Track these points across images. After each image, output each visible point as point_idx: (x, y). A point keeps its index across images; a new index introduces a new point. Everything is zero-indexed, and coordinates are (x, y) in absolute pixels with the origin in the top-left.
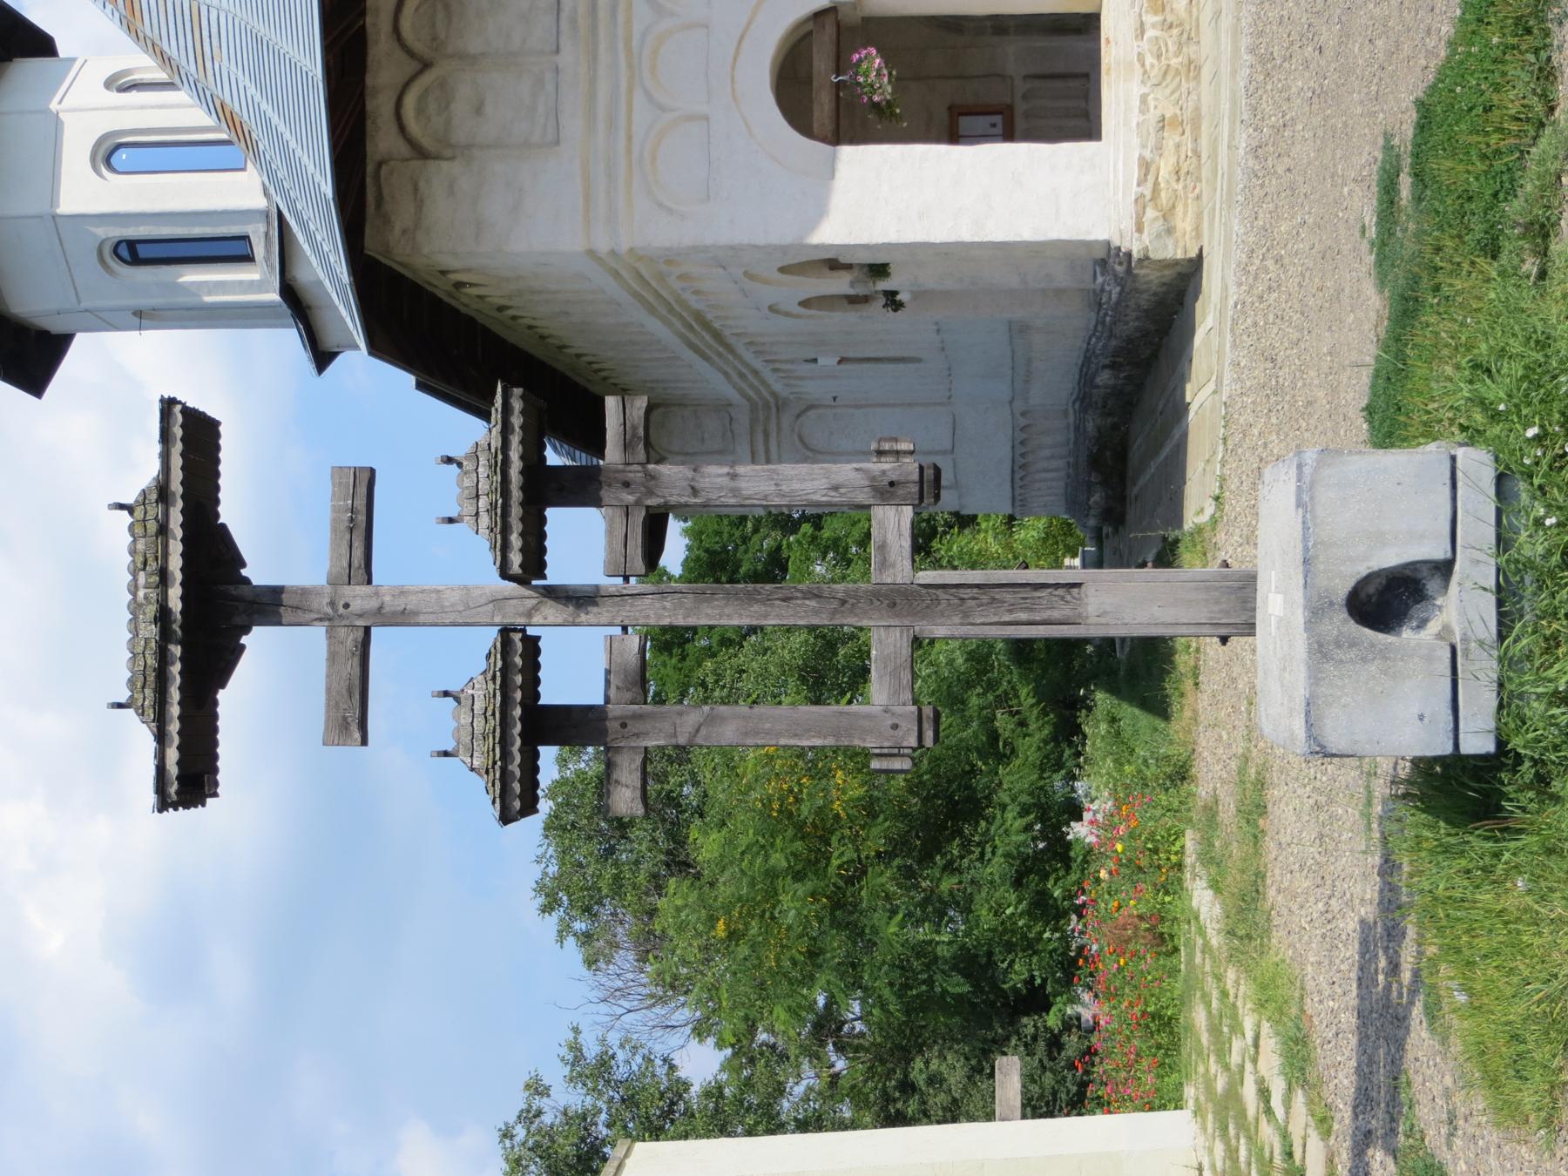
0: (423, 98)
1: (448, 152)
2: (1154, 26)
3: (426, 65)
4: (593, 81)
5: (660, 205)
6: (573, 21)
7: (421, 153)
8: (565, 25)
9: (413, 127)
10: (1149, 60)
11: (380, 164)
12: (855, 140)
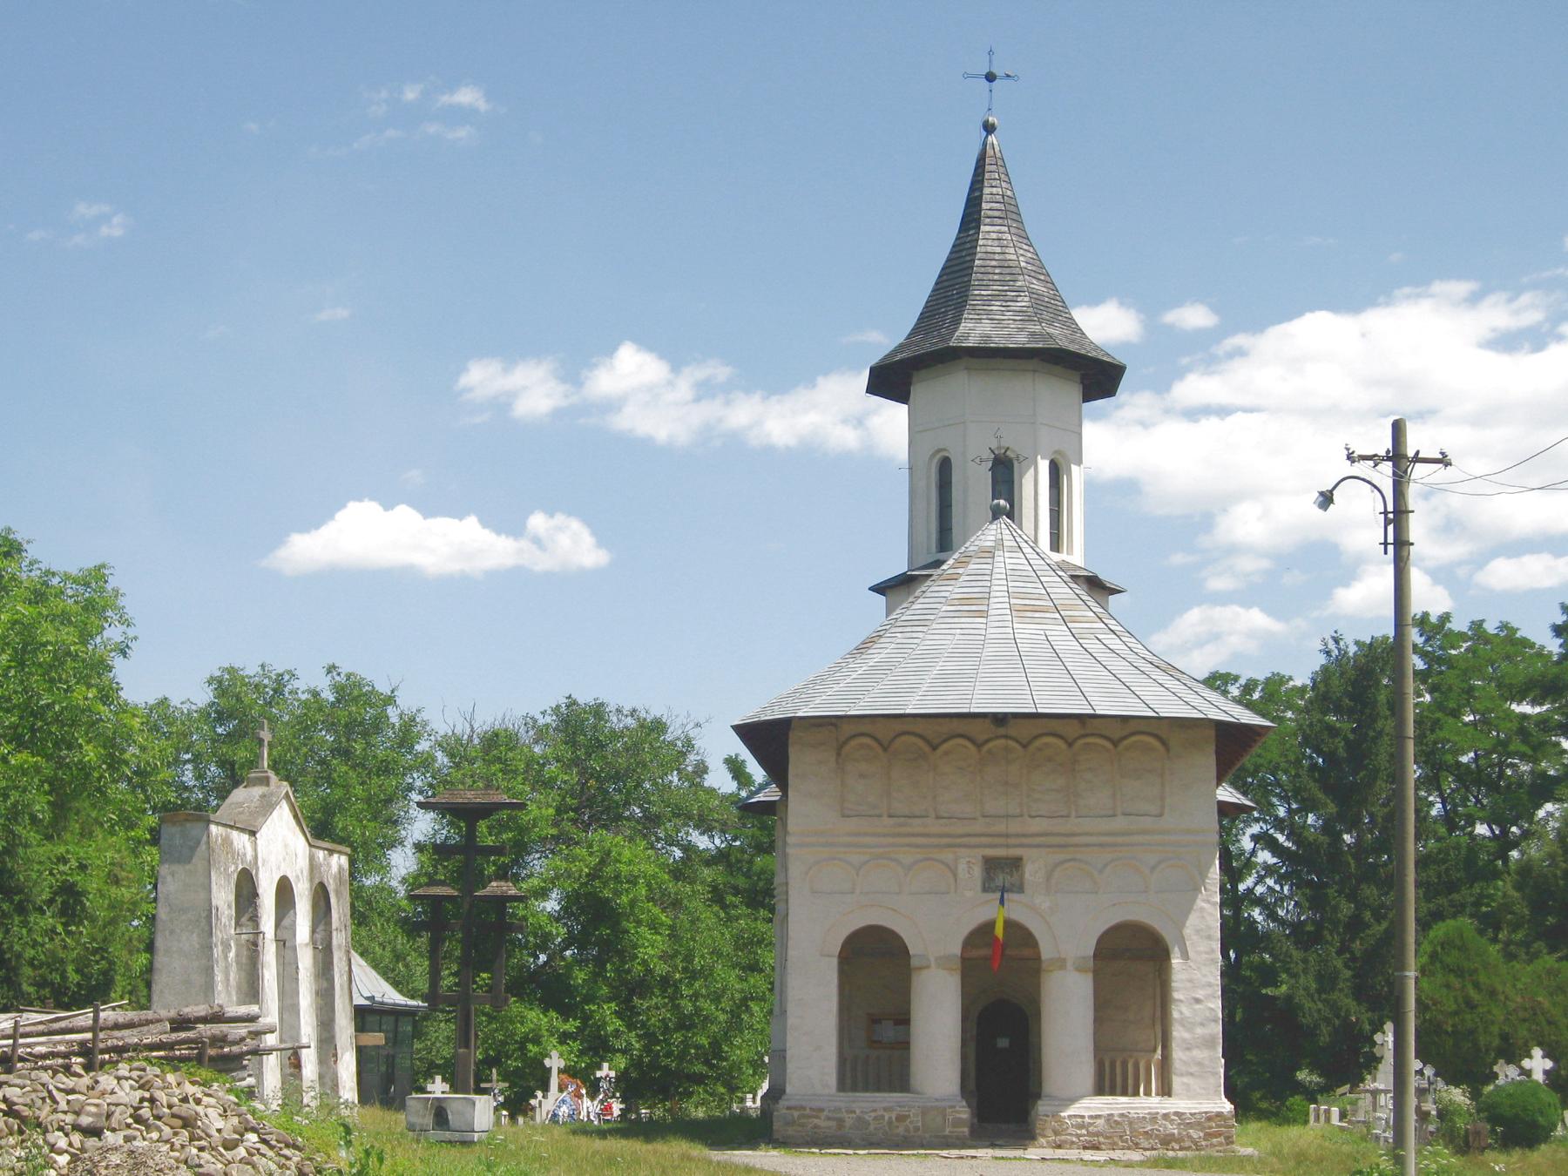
3: (885, 749)
6: (901, 825)
9: (853, 743)
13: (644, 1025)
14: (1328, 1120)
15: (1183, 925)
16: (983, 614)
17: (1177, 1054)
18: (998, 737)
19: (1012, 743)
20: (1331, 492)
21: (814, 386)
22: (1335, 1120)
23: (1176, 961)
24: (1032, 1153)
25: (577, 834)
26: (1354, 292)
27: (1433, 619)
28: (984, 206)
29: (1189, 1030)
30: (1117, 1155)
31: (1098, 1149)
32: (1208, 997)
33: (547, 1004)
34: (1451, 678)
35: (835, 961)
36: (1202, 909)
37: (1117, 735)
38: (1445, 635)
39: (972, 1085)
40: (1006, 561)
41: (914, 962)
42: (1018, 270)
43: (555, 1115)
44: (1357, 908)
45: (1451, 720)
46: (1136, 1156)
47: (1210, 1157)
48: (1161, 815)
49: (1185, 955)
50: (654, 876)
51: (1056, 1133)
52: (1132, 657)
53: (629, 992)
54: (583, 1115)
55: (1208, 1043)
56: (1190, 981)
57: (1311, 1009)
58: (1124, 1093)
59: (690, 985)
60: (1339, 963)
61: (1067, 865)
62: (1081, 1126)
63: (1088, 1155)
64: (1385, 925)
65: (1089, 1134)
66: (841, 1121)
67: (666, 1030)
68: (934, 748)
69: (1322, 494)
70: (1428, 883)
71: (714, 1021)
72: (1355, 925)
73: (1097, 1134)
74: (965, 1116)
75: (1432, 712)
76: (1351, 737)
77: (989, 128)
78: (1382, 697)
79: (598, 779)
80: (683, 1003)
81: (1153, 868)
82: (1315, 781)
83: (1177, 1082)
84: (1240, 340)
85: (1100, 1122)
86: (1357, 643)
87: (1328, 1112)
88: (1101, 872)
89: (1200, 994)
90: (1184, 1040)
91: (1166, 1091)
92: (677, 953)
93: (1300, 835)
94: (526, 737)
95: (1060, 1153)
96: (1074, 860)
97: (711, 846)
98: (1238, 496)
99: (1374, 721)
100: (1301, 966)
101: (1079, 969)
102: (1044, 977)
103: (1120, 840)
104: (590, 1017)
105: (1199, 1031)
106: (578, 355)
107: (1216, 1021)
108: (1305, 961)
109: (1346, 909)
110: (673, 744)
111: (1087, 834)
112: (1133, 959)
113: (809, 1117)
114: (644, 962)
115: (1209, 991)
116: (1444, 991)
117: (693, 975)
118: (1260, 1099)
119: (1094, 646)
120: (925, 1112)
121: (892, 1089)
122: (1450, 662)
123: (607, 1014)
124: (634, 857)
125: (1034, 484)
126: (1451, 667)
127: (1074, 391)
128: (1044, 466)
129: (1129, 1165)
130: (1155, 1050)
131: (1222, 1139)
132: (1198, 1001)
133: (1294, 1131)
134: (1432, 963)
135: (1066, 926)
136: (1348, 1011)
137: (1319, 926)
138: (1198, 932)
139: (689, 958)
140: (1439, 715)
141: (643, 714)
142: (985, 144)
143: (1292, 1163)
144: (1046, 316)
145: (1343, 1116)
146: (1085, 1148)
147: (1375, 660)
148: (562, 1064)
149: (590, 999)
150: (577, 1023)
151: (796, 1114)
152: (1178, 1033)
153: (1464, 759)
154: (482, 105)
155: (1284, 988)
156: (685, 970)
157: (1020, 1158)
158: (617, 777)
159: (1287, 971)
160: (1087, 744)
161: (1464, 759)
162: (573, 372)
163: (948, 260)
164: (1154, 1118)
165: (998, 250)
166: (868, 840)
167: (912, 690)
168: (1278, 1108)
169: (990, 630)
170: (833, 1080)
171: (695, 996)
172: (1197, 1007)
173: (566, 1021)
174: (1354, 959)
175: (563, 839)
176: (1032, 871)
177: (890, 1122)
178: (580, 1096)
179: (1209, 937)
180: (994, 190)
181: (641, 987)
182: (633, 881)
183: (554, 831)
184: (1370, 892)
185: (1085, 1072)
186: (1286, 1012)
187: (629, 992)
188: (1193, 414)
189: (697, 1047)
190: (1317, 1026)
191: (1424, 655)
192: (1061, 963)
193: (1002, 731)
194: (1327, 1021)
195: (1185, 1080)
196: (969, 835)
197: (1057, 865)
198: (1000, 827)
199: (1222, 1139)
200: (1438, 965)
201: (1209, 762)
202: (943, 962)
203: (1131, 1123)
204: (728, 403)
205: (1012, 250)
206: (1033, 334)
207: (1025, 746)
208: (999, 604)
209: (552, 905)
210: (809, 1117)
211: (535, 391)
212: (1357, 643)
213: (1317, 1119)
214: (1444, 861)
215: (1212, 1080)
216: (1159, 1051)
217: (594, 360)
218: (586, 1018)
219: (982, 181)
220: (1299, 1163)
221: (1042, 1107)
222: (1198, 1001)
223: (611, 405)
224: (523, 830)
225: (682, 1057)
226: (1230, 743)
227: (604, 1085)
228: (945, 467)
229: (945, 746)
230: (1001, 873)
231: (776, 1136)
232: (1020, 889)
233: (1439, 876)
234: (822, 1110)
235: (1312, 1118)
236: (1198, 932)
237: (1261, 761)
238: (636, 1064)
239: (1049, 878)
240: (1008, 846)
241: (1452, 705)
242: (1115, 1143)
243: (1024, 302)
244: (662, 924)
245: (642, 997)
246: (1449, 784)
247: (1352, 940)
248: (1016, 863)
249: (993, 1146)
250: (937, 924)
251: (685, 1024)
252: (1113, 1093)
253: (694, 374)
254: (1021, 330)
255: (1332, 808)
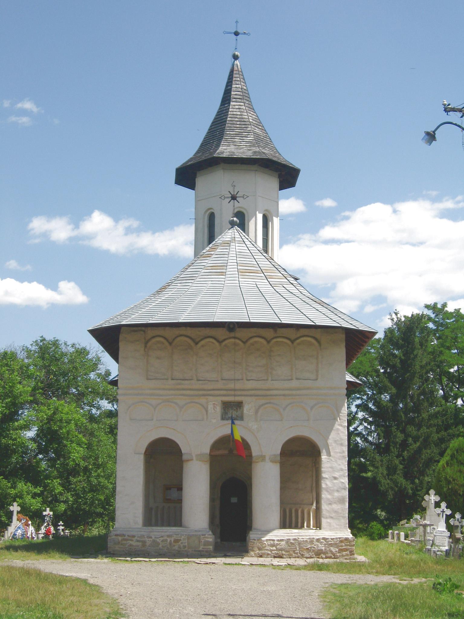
0: (163, 343)
1: (146, 350)
2: (171, 541)
3: (170, 344)
4: (164, 389)
5: (129, 407)
6: (180, 384)
7: (146, 343)
8: (179, 381)
9: (154, 340)
10: (162, 539)
11: (144, 331)
12: (251, 453)
13: (75, 490)
14: (399, 538)
15: (328, 438)
16: (222, 274)
17: (324, 507)
18: (230, 338)
19: (237, 341)
20: (434, 132)
21: (174, 230)
22: (402, 538)
23: (324, 457)
24: (246, 561)
25: (41, 399)
26: (392, 196)
27: (439, 306)
28: (233, 93)
29: (330, 494)
30: (291, 561)
31: (282, 557)
32: (340, 476)
33: (27, 480)
34: (447, 332)
35: (142, 457)
36: (338, 429)
37: (293, 337)
38: (445, 313)
39: (217, 521)
40: (236, 247)
41: (184, 457)
42: (248, 123)
43: (15, 535)
44: (405, 436)
45: (447, 351)
46: (301, 562)
47: (342, 563)
48: (317, 379)
49: (329, 454)
50: (79, 420)
51: (260, 549)
52: (301, 296)
53: (68, 474)
54: (29, 534)
55: (341, 501)
56: (331, 468)
57: (385, 483)
58: (296, 527)
59: (96, 471)
60: (397, 462)
61: (266, 406)
62: (273, 545)
63: (276, 562)
64: (418, 444)
65: (277, 550)
66: (144, 542)
67: (84, 492)
68: (197, 343)
69: (428, 134)
70: (438, 425)
71: (106, 488)
72: (404, 445)
73: (281, 550)
74: (211, 540)
75: (439, 348)
76: (403, 358)
77: (236, 57)
78: (417, 340)
79: (55, 375)
80: (92, 479)
81: (312, 408)
82: (387, 378)
83: (324, 522)
84: (347, 213)
85: (283, 543)
86: (405, 316)
87: (398, 535)
88: (284, 409)
89: (337, 475)
90: (328, 499)
91: (318, 526)
92: (90, 457)
93: (379, 403)
94: (21, 355)
95: (261, 560)
96: (270, 403)
97: (113, 409)
98: (344, 277)
99: (413, 351)
100: (380, 463)
101: (273, 461)
102: (253, 465)
103: (294, 392)
104: (47, 486)
105: (336, 494)
106: (78, 217)
107: (345, 489)
108: (382, 461)
109: (400, 437)
110: (91, 360)
111: (277, 389)
112: (302, 456)
113: (127, 540)
114: (74, 460)
115: (341, 473)
116: (458, 474)
117: (98, 466)
118: (359, 523)
119: (280, 290)
120: (189, 537)
121: (175, 526)
122: (446, 326)
123: (56, 485)
124: (67, 409)
125: (256, 223)
126: (447, 328)
127: (274, 183)
128: (260, 217)
129: (298, 568)
130: (312, 504)
131: (348, 552)
132: (335, 478)
133: (382, 544)
134: (452, 459)
135: (265, 438)
136: (401, 484)
137: (388, 446)
138: (335, 441)
139: (97, 459)
140: (442, 349)
141: (77, 346)
142: (233, 65)
143: (387, 567)
144: (261, 144)
145: (406, 537)
146: (275, 557)
147: (414, 323)
148: (19, 509)
149: (47, 477)
150: (41, 489)
151: (120, 538)
152: (325, 495)
153: (452, 370)
154: (35, 109)
155: (369, 474)
156: (94, 464)
157: (239, 564)
158: (64, 374)
159: (373, 466)
160: (277, 342)
161: (452, 370)
162: (76, 222)
163: (215, 119)
164: (311, 541)
165: (239, 113)
166: (161, 392)
167: (184, 310)
168: (367, 527)
169: (227, 282)
170: (140, 520)
171: (99, 476)
172: (335, 481)
173: (36, 488)
174: (404, 460)
175: (35, 402)
176: (247, 409)
177: (170, 543)
178: (28, 525)
179: (342, 445)
180: (238, 86)
181: (75, 472)
182: (68, 422)
183: (32, 398)
184: (411, 429)
185: (275, 517)
186: (374, 483)
187: (68, 474)
188: (327, 242)
189: (100, 500)
190: (387, 491)
191: (434, 322)
192: (263, 458)
193: (232, 334)
194: (392, 489)
195: (328, 520)
196: (214, 390)
197: (260, 407)
198: (231, 386)
199: (348, 552)
200: (455, 461)
201: (341, 353)
202: (200, 457)
203: (299, 544)
204: (138, 236)
205: (246, 114)
206: (255, 152)
207: (244, 343)
208: (232, 269)
209: (31, 434)
210: (127, 540)
211: (60, 230)
212: (405, 316)
213: (393, 538)
214: (445, 415)
215: (343, 521)
216: (315, 504)
217: (85, 217)
218: (45, 486)
219: (232, 82)
220: (390, 567)
221: (252, 535)
222: (335, 478)
223: (90, 237)
224: (15, 397)
225: (92, 503)
226: (355, 340)
227: (47, 519)
228: (212, 217)
229: (203, 342)
230: (232, 410)
231: (109, 550)
232: (241, 418)
233: (443, 422)
234: (134, 536)
235: (390, 536)
236: (335, 441)
237: (361, 370)
238: (70, 508)
239: (257, 412)
240: (235, 395)
241: (448, 344)
242: (291, 555)
243: (251, 138)
244: (83, 443)
245: (74, 477)
246: (445, 380)
247: (403, 451)
248: (239, 405)
249: (225, 556)
250: (197, 436)
251: (94, 489)
252: (290, 527)
253: (124, 224)
254: (250, 150)
255: (394, 390)
